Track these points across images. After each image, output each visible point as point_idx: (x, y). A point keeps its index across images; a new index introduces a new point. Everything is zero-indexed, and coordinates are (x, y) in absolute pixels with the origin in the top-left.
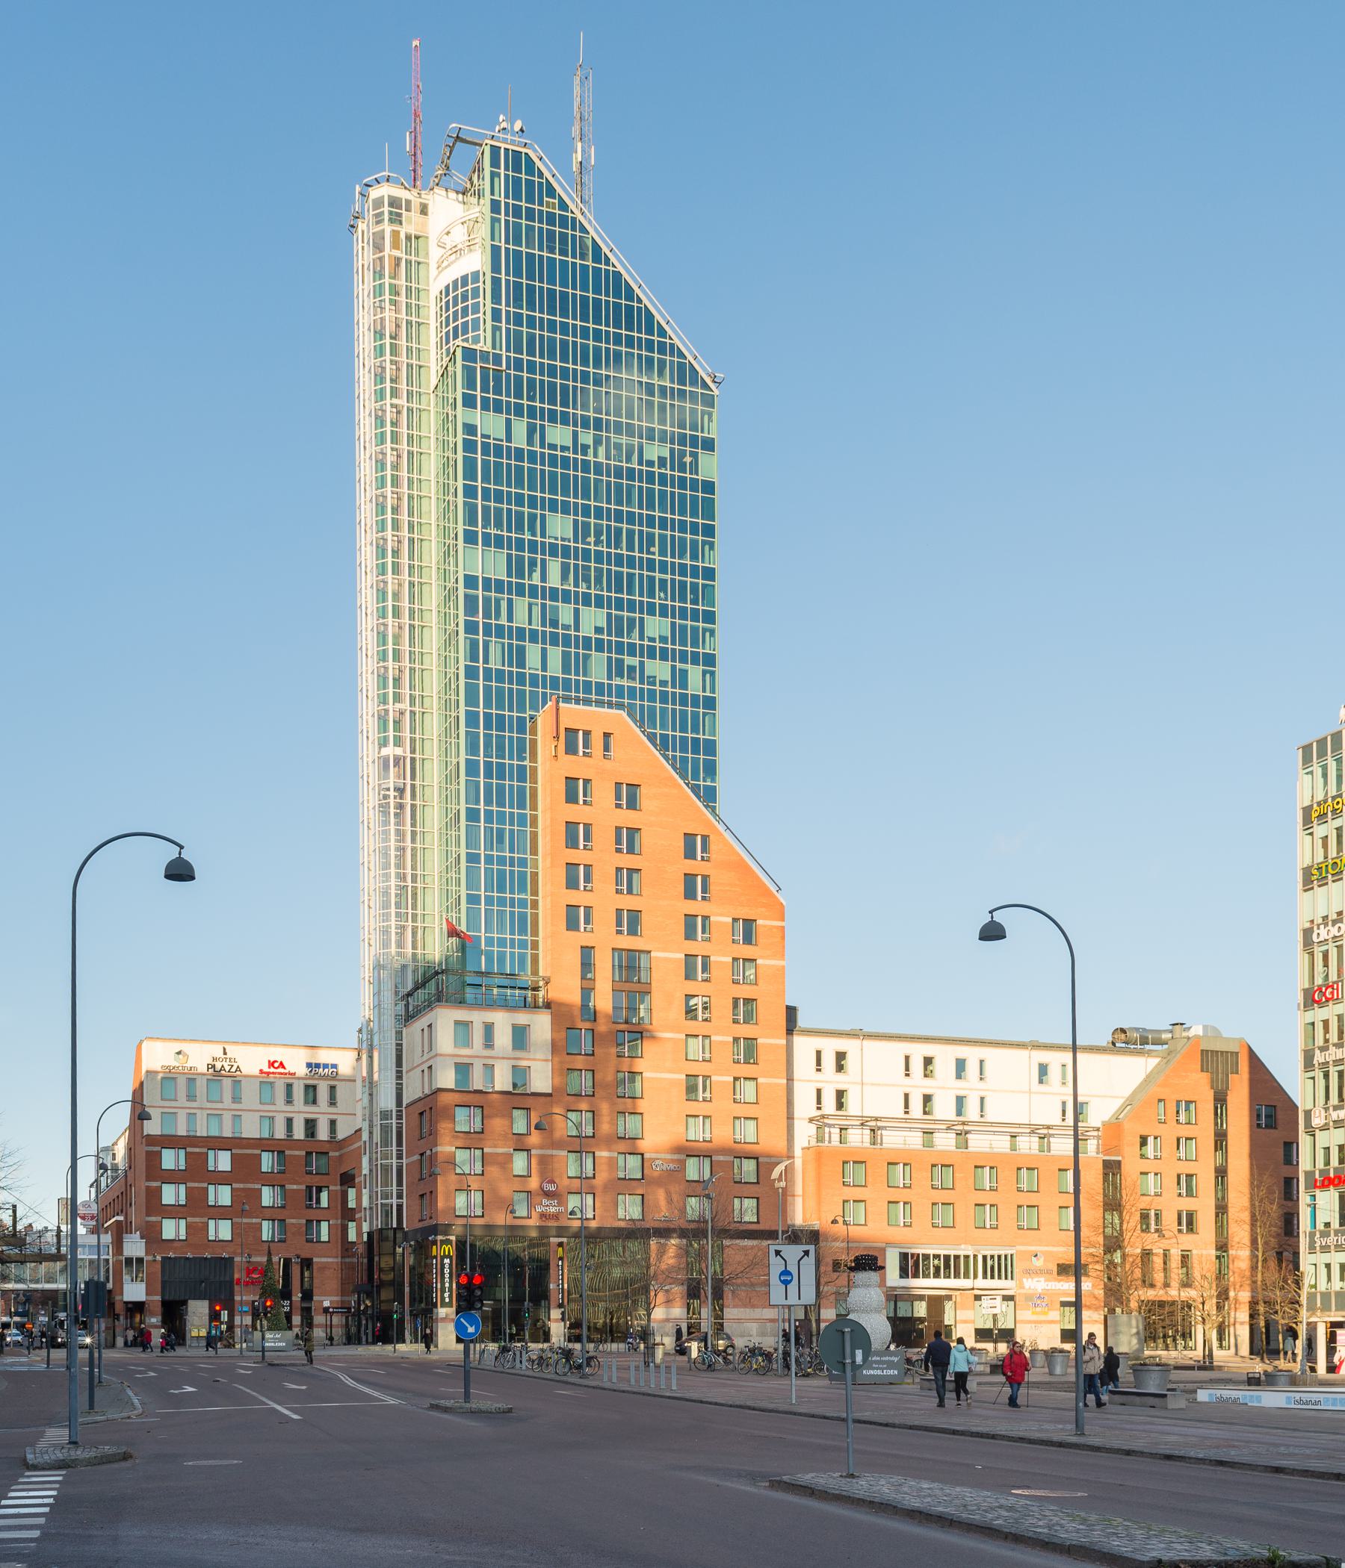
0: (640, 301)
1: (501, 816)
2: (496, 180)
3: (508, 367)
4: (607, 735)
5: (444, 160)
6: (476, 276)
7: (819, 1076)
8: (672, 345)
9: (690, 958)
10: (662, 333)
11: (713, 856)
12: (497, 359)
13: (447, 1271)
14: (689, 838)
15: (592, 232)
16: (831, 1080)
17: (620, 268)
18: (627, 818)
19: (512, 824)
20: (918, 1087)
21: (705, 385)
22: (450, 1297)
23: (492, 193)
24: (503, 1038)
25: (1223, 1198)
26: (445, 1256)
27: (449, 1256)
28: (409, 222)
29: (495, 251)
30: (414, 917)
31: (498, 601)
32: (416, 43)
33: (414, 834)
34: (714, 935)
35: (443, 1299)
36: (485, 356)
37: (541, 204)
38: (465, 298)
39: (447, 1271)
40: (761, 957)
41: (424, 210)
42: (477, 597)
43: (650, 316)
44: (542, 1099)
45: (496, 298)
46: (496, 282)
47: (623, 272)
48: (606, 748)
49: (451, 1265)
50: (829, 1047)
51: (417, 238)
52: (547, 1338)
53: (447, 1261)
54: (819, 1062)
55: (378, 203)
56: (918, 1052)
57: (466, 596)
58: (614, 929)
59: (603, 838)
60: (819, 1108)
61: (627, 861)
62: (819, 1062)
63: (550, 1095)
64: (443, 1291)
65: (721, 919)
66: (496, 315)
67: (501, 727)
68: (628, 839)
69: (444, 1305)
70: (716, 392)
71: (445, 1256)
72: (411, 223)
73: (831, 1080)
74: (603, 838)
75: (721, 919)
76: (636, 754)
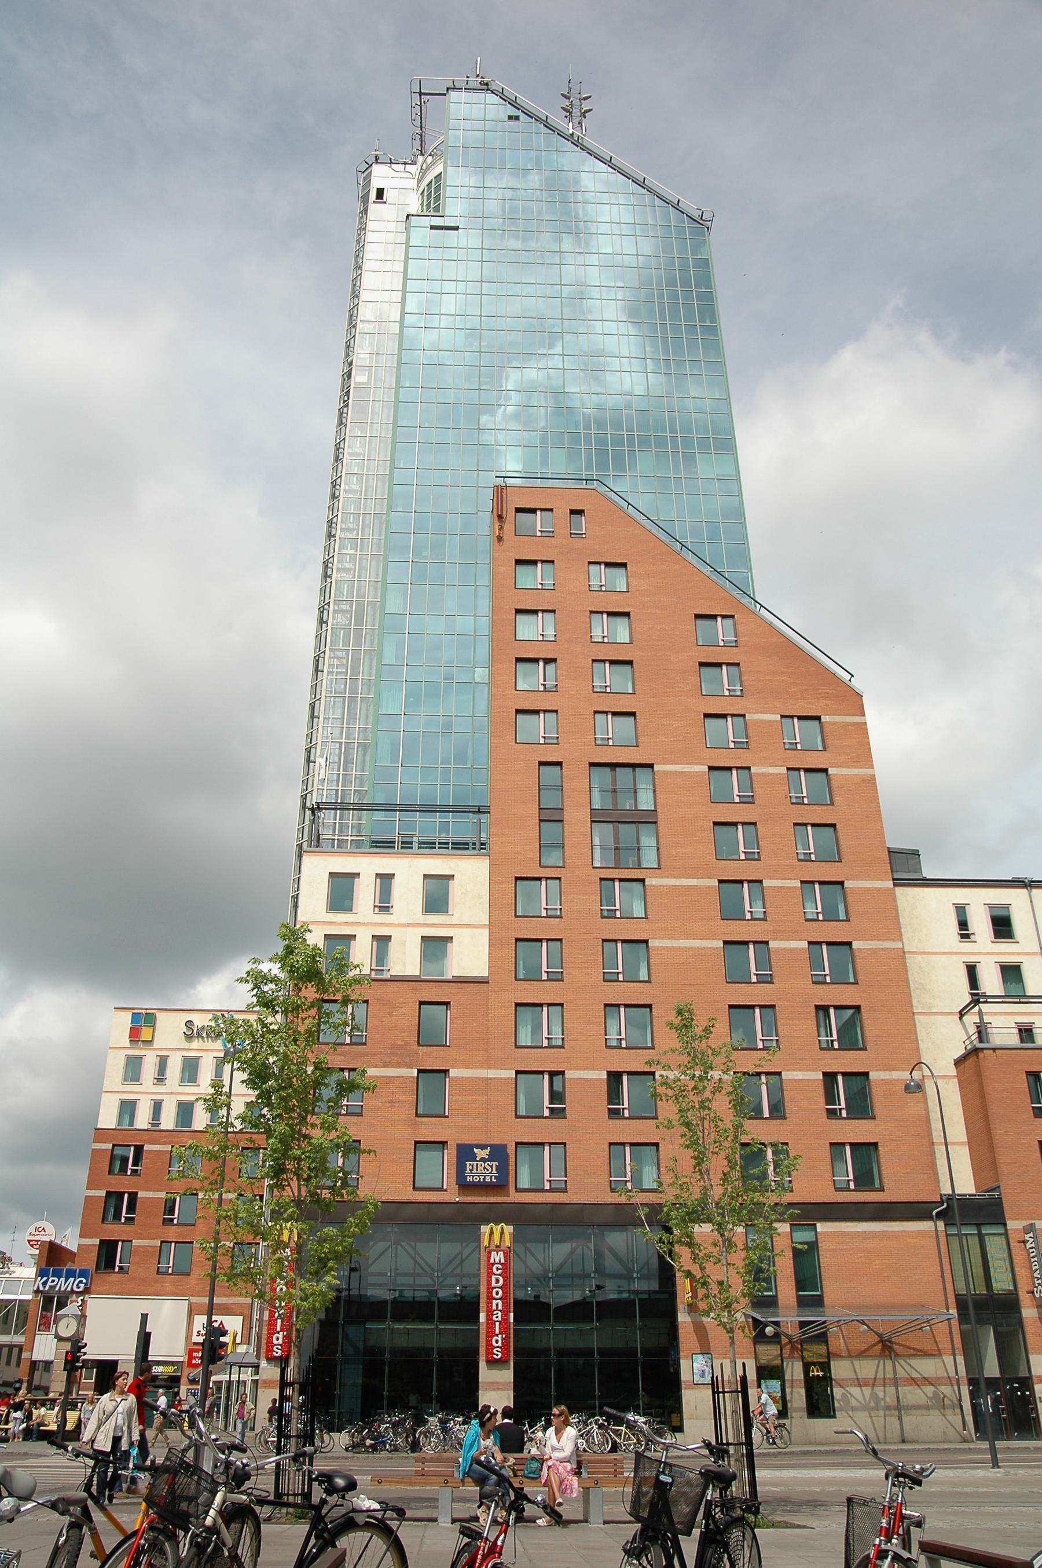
24: (408, 892)
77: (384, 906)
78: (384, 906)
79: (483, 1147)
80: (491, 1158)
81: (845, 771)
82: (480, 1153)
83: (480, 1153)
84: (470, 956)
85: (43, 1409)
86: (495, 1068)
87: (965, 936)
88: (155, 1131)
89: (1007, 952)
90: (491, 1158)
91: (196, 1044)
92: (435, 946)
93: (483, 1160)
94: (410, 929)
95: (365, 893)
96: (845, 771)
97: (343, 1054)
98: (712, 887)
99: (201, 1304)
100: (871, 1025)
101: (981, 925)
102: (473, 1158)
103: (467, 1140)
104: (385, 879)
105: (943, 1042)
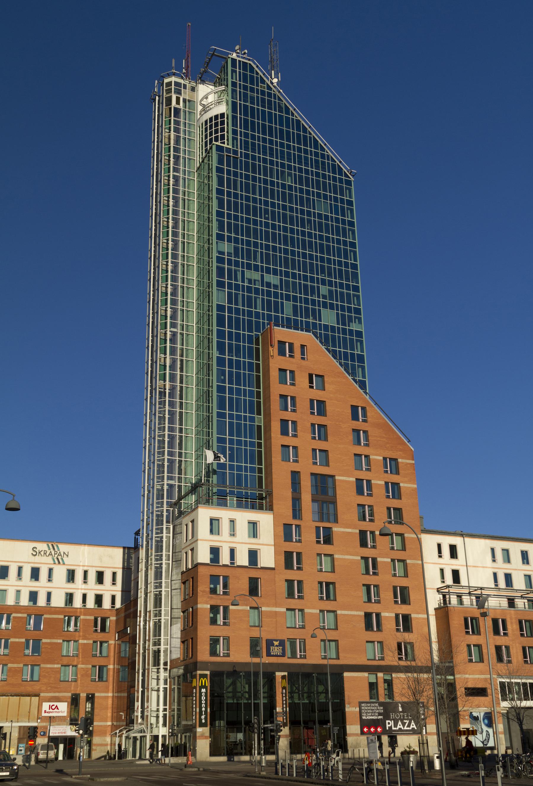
0: (310, 134)
1: (238, 391)
2: (234, 74)
3: (241, 156)
4: (303, 347)
5: (205, 70)
6: (222, 115)
7: (440, 560)
8: (328, 156)
9: (359, 481)
10: (323, 149)
11: (369, 419)
12: (235, 152)
13: (203, 698)
14: (354, 409)
15: (284, 101)
16: (449, 564)
17: (299, 118)
18: (317, 394)
19: (245, 396)
20: (502, 568)
21: (346, 176)
22: (206, 718)
23: (232, 78)
24: (242, 528)
25: (129, 557)
26: (201, 687)
27: (205, 687)
28: (185, 93)
29: (234, 105)
30: (180, 455)
31: (236, 271)
32: (190, 24)
33: (181, 404)
34: (373, 467)
35: (200, 720)
36: (228, 150)
37: (257, 86)
38: (216, 132)
39: (203, 698)
40: (402, 482)
41: (193, 89)
42: (224, 268)
43: (316, 141)
44: (269, 572)
45: (234, 124)
46: (234, 118)
47: (301, 120)
48: (303, 353)
49: (206, 693)
50: (446, 541)
51: (189, 101)
52: (275, 752)
53: (203, 690)
54: (440, 551)
55: (169, 84)
56: (499, 545)
57: (218, 267)
58: (311, 461)
59: (303, 405)
60: (443, 582)
61: (318, 420)
62: (440, 551)
63: (273, 569)
64: (201, 714)
65: (377, 458)
66: (235, 132)
67: (238, 339)
68: (320, 407)
69: (202, 725)
70: (352, 179)
71: (201, 687)
72: (186, 94)
73: (449, 564)
74: (303, 405)
75: (377, 458)
76: (320, 358)
77: (233, 534)
78: (233, 534)
79: (276, 641)
80: (280, 645)
81: (406, 485)
82: (276, 643)
83: (276, 643)
84: (267, 558)
85: (477, 741)
86: (279, 607)
87: (440, 557)
88: (49, 609)
89: (455, 564)
90: (280, 645)
91: (38, 559)
92: (253, 555)
93: (277, 646)
94: (243, 545)
95: (225, 527)
96: (406, 485)
97: (221, 599)
98: (356, 533)
99: (464, 723)
100: (413, 596)
101: (446, 551)
102: (273, 645)
103: (270, 637)
104: (232, 521)
105: (434, 600)
